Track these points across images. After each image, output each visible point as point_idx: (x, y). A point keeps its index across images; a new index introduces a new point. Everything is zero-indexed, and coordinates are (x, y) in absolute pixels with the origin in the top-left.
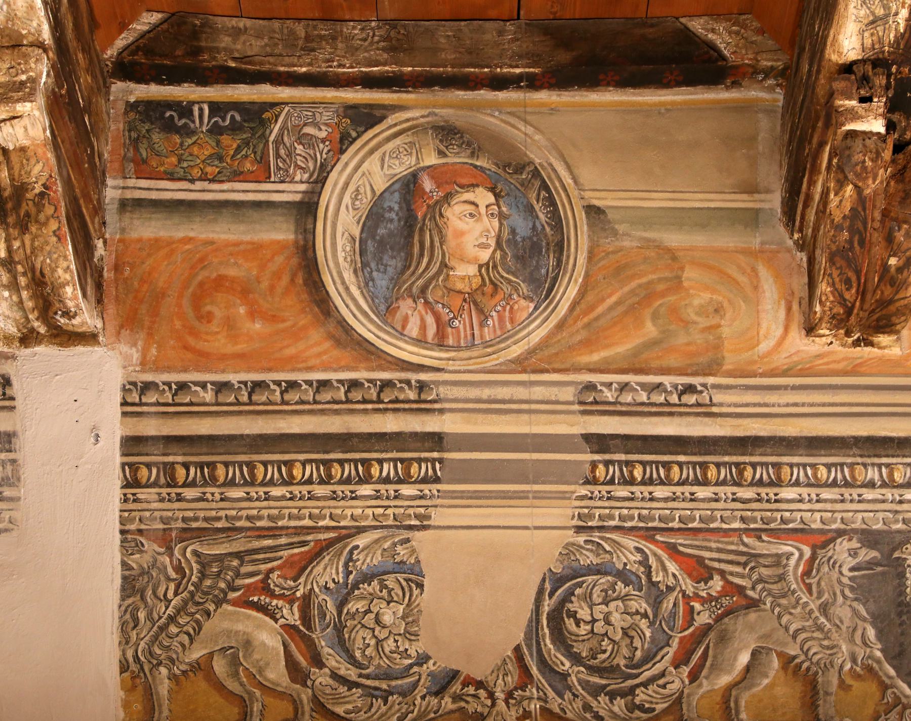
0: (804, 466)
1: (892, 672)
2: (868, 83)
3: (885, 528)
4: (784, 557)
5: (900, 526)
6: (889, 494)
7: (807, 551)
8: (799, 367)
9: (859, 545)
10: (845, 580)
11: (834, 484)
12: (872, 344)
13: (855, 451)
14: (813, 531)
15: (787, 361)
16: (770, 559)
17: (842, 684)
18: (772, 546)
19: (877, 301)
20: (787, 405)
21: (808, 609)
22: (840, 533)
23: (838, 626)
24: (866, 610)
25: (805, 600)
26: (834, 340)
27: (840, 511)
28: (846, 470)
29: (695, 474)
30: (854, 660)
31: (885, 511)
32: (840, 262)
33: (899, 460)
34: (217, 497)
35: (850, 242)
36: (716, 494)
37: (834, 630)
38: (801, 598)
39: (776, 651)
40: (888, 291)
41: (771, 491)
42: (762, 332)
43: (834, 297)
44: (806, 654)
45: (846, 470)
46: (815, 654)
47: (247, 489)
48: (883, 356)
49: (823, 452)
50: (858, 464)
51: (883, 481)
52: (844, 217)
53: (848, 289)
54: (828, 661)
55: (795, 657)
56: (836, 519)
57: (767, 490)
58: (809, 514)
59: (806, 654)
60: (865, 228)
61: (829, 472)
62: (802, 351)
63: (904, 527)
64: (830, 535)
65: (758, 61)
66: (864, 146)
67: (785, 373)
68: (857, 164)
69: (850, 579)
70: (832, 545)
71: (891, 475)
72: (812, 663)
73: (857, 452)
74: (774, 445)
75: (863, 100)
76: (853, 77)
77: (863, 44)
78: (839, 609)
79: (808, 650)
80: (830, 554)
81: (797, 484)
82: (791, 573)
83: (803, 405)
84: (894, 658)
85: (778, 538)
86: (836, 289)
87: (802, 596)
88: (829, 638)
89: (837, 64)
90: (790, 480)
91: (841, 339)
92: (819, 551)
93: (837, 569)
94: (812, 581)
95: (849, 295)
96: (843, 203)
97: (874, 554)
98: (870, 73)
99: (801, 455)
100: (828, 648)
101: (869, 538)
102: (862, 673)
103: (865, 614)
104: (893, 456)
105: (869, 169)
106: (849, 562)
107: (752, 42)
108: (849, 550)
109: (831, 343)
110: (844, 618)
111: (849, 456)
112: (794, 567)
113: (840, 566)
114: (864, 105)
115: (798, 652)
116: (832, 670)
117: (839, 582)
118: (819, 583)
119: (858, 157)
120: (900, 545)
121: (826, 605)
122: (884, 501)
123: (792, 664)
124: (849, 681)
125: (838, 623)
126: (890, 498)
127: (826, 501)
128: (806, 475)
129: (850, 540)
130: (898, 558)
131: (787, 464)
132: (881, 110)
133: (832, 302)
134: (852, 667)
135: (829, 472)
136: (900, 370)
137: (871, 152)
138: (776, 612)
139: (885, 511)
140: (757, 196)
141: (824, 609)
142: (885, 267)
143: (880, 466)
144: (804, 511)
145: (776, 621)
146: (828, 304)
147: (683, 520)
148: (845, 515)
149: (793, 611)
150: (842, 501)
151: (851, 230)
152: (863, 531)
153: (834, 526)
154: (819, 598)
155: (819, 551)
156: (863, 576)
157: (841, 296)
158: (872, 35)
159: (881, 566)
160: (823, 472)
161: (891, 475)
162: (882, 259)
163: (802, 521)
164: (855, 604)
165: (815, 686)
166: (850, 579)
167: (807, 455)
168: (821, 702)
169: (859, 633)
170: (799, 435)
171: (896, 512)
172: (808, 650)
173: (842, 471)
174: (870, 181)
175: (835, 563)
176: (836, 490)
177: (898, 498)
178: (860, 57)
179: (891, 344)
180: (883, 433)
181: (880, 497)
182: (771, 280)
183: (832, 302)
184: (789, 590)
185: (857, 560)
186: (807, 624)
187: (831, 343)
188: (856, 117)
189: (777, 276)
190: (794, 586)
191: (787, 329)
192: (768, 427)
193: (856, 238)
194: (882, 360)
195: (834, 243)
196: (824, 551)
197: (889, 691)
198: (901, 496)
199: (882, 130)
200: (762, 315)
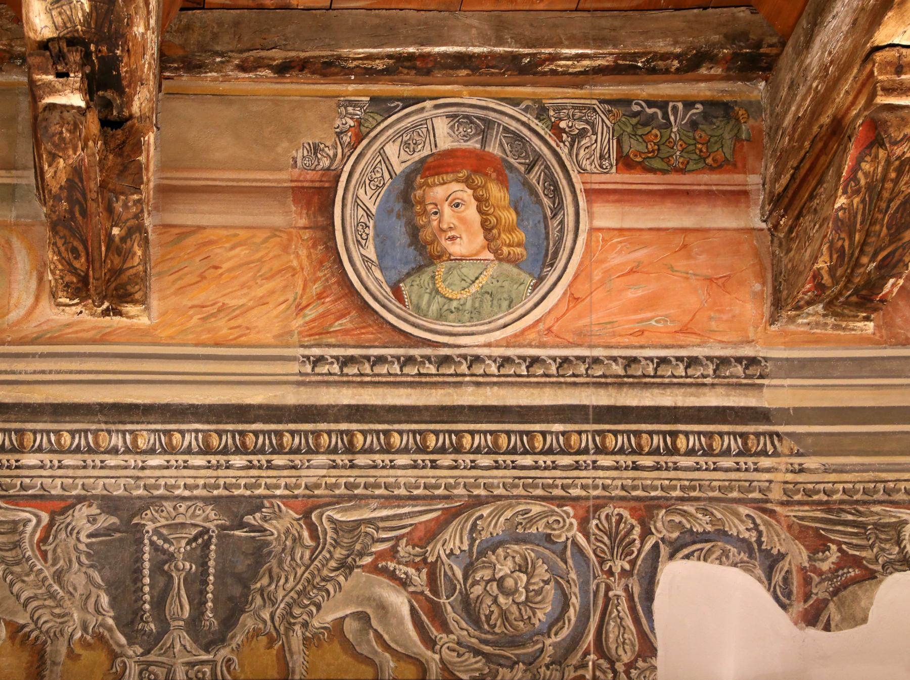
0: (48, 432)
1: (123, 640)
2: (64, 59)
3: (126, 493)
4: (21, 524)
5: (140, 492)
6: (131, 460)
7: (45, 518)
8: (48, 336)
9: (98, 511)
10: (82, 547)
11: (78, 450)
12: (120, 314)
13: (100, 417)
14: (52, 497)
15: (36, 329)
16: (6, 526)
17: (72, 655)
18: (9, 513)
19: (109, 270)
20: (35, 372)
21: (42, 576)
22: (80, 499)
23: (71, 594)
24: (101, 577)
25: (39, 567)
26: (83, 310)
27: (81, 477)
28: (90, 437)
29: (271, 442)
30: (85, 628)
31: (127, 477)
32: (63, 231)
33: (144, 426)
34: (181, 463)
35: (71, 211)
36: (456, 461)
37: (66, 598)
38: (35, 565)
39: (4, 620)
40: (117, 260)
41: (12, 458)
42: (13, 302)
43: (62, 265)
44: (36, 623)
45: (90, 437)
46: (45, 622)
47: (167, 457)
48: (132, 325)
49: (67, 419)
50: (103, 430)
51: (127, 447)
52: (61, 188)
53: (76, 258)
54: (58, 630)
55: (24, 626)
56: (77, 485)
57: (9, 456)
58: (50, 480)
59: (36, 623)
60: (85, 199)
61: (330, 438)
62: (52, 320)
63: (145, 493)
64: (70, 501)
65: (12, 47)
66: (62, 118)
67: (34, 342)
68: (54, 135)
69: (87, 545)
70: (71, 511)
71: (135, 441)
72: (41, 632)
73: (102, 418)
74: (18, 411)
75: (59, 75)
76: (48, 53)
77: (54, 23)
78: (74, 576)
79: (38, 618)
80: (68, 520)
81: (40, 450)
82: (27, 540)
83: (50, 372)
84: (127, 625)
85: (17, 505)
86: (63, 258)
87: (37, 563)
88: (61, 606)
89: (36, 41)
90: (33, 446)
91: (91, 309)
92: (57, 518)
93: (74, 535)
94: (47, 548)
95: (80, 264)
96: (59, 174)
97: (114, 520)
98: (65, 50)
99: (45, 422)
100: (59, 616)
101: (109, 504)
102: (92, 641)
103: (99, 580)
104: (138, 423)
105: (68, 140)
106: (88, 529)
107: (7, 30)
108: (88, 516)
109: (81, 312)
110: (77, 586)
111: (94, 422)
112: (31, 533)
113: (78, 533)
114: (61, 80)
115: (28, 620)
116: (61, 639)
117: (76, 549)
118: (55, 550)
119: (55, 129)
120: (140, 511)
121: (61, 572)
122: (126, 468)
123: (20, 634)
124: (78, 650)
125: (71, 589)
126: (133, 464)
127: (68, 467)
128: (50, 441)
129: (90, 506)
130: (137, 524)
131: (31, 431)
132: (78, 85)
133: (61, 271)
134: (82, 635)
135: (73, 438)
136: (149, 339)
137: (68, 123)
138: (8, 580)
139: (127, 477)
140: (14, 172)
141: (59, 576)
142: (110, 237)
143: (124, 433)
144: (45, 477)
145: (8, 589)
146: (58, 272)
147: (86, 487)
148: (86, 481)
149: (26, 579)
150: (85, 467)
151: (69, 200)
152: (103, 497)
153: (74, 493)
154: (53, 565)
155: (57, 518)
156: (101, 542)
157: (70, 264)
158: (60, 13)
159: (120, 532)
160: (66, 439)
161: (135, 441)
162: (106, 230)
163: (42, 487)
164: (91, 571)
165: (43, 656)
166: (87, 545)
167: (51, 422)
168: (47, 673)
169: (93, 600)
170: (44, 402)
171: (138, 478)
172: (38, 618)
173: (86, 438)
174: (71, 152)
175: (73, 529)
176: (79, 456)
177: (140, 464)
178: (55, 35)
179: (138, 313)
180: (129, 400)
181: (123, 463)
182: (24, 252)
183: (61, 271)
184: (24, 557)
185: (96, 527)
186: (40, 591)
187: (81, 312)
188: (53, 91)
189: (30, 249)
190: (29, 553)
191: (37, 298)
192: (13, 394)
193: (77, 209)
194: (131, 330)
195: (55, 212)
196: (62, 517)
197: (119, 660)
198: (144, 462)
199: (83, 104)
200: (14, 285)
